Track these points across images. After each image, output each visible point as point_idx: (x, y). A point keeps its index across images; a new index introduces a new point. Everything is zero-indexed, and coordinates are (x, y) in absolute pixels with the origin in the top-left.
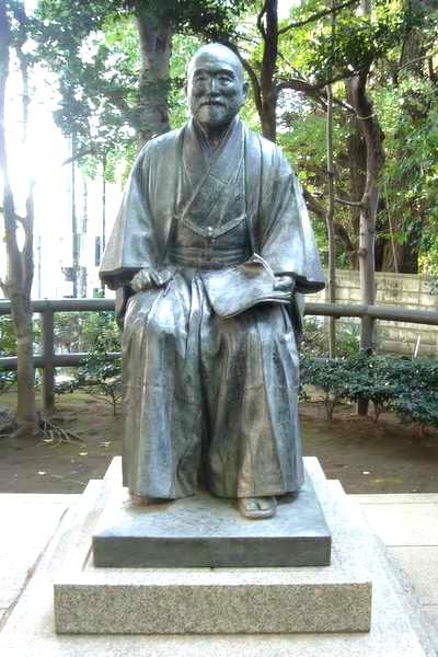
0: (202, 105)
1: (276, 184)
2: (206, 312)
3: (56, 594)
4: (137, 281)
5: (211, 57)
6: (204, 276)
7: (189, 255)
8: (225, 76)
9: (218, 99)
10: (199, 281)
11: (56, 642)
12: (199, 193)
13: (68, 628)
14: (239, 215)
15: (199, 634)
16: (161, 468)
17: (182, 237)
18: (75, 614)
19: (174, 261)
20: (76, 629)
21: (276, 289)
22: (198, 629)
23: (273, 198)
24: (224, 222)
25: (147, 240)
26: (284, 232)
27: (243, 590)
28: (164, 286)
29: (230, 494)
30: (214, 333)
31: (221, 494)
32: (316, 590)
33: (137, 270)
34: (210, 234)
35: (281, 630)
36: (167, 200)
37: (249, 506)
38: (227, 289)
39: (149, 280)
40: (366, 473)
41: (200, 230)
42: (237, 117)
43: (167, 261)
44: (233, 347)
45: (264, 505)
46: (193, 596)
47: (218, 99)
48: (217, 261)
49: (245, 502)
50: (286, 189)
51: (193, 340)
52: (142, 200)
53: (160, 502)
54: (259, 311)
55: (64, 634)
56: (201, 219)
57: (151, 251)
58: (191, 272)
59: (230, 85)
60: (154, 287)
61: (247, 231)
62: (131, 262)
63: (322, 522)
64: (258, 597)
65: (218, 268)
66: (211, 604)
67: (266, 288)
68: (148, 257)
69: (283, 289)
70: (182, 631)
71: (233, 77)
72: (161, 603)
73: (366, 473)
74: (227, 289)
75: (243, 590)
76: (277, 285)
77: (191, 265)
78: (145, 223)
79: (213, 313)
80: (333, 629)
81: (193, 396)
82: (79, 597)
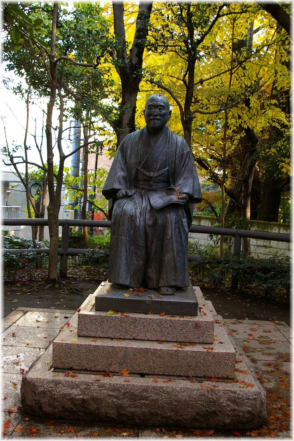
0: (151, 119)
1: (182, 155)
2: (149, 208)
3: (79, 318)
4: (120, 194)
5: (156, 99)
6: (148, 193)
7: (142, 185)
8: (161, 108)
9: (157, 117)
10: (146, 195)
11: (77, 339)
12: (148, 158)
13: (83, 333)
14: (165, 168)
15: (139, 340)
16: (126, 272)
17: (140, 177)
18: (34, 408)
19: (136, 187)
20: (86, 334)
21: (179, 199)
22: (139, 338)
23: (181, 160)
24: (158, 171)
25: (124, 178)
26: (185, 175)
27: (158, 321)
28: (131, 196)
29: (155, 286)
30: (152, 216)
31: (151, 287)
32: (190, 323)
33: (119, 190)
34: (152, 175)
35: (174, 340)
36: (133, 161)
37: (164, 290)
38: (158, 200)
39: (125, 193)
40: (37, 81)
41: (148, 174)
42: (167, 125)
43: (132, 187)
44: (160, 222)
45: (170, 290)
46: (136, 322)
47: (157, 117)
48: (154, 187)
49: (162, 288)
50: (186, 158)
51: (142, 219)
52: (123, 161)
53: (125, 288)
54: (171, 206)
55: (81, 336)
56: (149, 169)
57: (126, 182)
58: (143, 192)
59: (163, 111)
60: (127, 196)
61: (168, 175)
62: (117, 186)
63: (196, 300)
64: (165, 325)
65: (155, 191)
66: (144, 326)
67: (174, 198)
68: (124, 184)
69: (183, 199)
70: (131, 338)
71: (165, 108)
72: (123, 325)
73: (37, 81)
74: (158, 200)
75: (158, 321)
76: (179, 197)
77: (143, 189)
78: (124, 170)
79: (152, 207)
80: (197, 342)
81: (142, 242)
82: (88, 320)
